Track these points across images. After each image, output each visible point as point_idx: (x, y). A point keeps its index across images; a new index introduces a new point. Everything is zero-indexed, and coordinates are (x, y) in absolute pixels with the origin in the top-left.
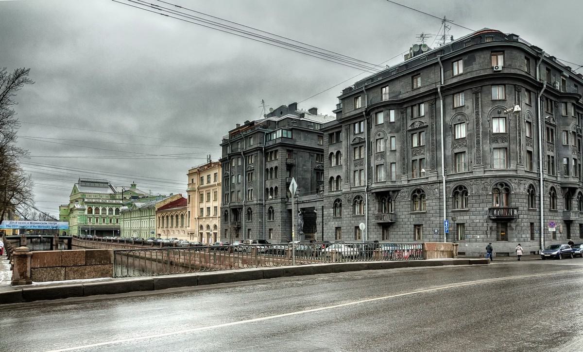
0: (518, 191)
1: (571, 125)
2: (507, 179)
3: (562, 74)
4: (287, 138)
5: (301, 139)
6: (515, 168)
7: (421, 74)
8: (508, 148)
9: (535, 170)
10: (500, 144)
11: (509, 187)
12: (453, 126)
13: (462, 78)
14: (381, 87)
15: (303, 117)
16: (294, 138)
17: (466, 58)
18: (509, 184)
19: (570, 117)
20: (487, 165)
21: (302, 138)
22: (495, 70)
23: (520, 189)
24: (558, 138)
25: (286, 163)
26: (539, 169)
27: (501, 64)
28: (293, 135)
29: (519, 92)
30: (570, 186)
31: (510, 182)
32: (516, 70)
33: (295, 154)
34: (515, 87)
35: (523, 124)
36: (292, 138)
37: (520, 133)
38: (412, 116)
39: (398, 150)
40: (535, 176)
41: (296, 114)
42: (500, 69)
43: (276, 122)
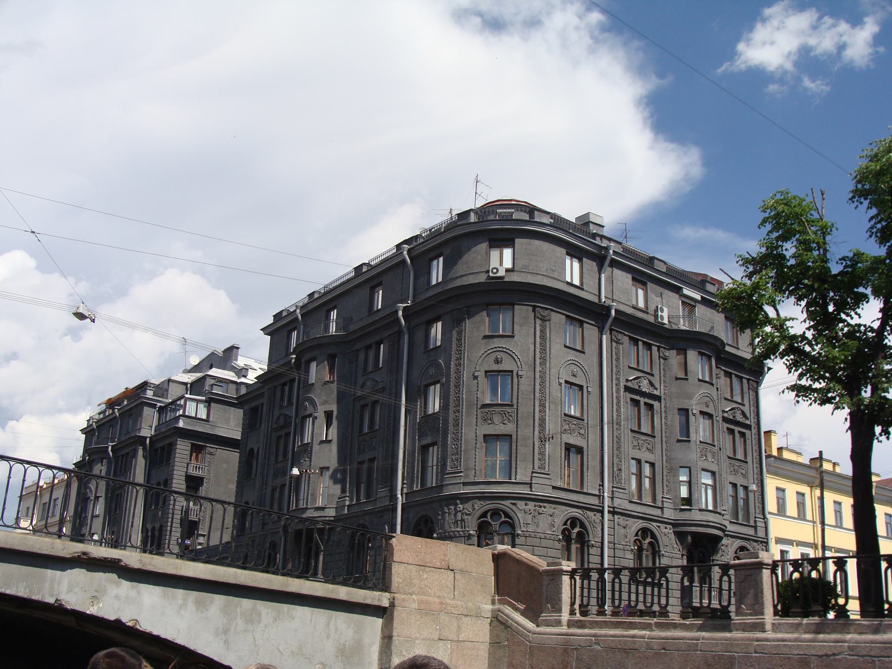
0: (531, 528)
1: (697, 397)
2: (507, 503)
3: (681, 293)
4: (196, 418)
5: (228, 424)
6: (528, 480)
7: (384, 282)
8: (514, 437)
9: (591, 486)
10: (497, 427)
11: (512, 520)
12: (422, 389)
13: (439, 290)
14: (326, 308)
15: (245, 376)
16: (211, 419)
17: (447, 251)
18: (511, 514)
19: (692, 379)
20: (469, 472)
21: (232, 420)
22: (491, 274)
23: (537, 526)
24: (669, 423)
25: (186, 473)
26: (602, 485)
27: (508, 263)
28: (212, 412)
29: (544, 320)
30: (693, 529)
31: (513, 507)
32: (539, 277)
33: (211, 454)
34: (534, 311)
35: (555, 385)
36: (207, 420)
37: (543, 406)
38: (365, 369)
39: (335, 440)
40: (594, 501)
41: (233, 369)
42: (501, 273)
43: (186, 384)
